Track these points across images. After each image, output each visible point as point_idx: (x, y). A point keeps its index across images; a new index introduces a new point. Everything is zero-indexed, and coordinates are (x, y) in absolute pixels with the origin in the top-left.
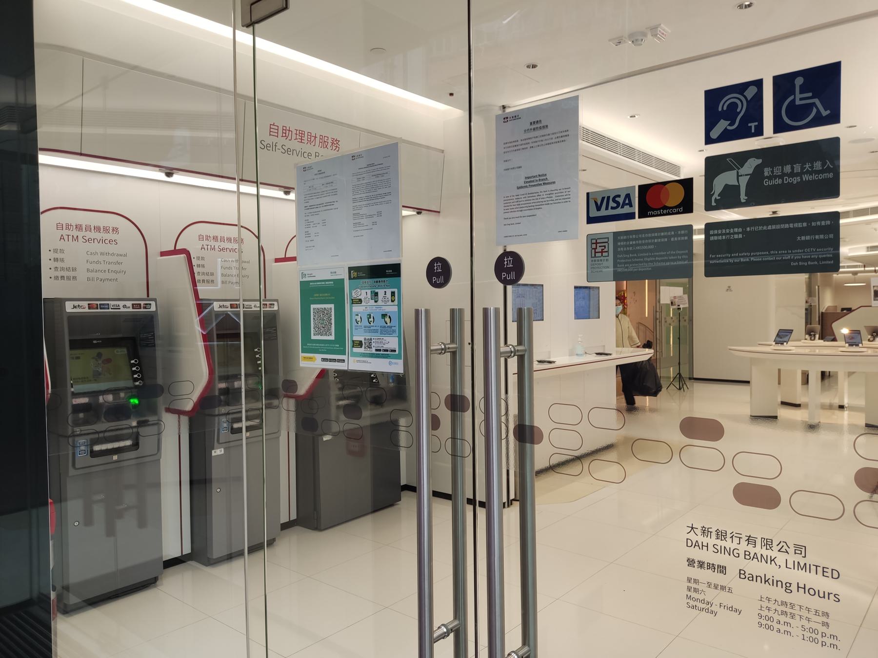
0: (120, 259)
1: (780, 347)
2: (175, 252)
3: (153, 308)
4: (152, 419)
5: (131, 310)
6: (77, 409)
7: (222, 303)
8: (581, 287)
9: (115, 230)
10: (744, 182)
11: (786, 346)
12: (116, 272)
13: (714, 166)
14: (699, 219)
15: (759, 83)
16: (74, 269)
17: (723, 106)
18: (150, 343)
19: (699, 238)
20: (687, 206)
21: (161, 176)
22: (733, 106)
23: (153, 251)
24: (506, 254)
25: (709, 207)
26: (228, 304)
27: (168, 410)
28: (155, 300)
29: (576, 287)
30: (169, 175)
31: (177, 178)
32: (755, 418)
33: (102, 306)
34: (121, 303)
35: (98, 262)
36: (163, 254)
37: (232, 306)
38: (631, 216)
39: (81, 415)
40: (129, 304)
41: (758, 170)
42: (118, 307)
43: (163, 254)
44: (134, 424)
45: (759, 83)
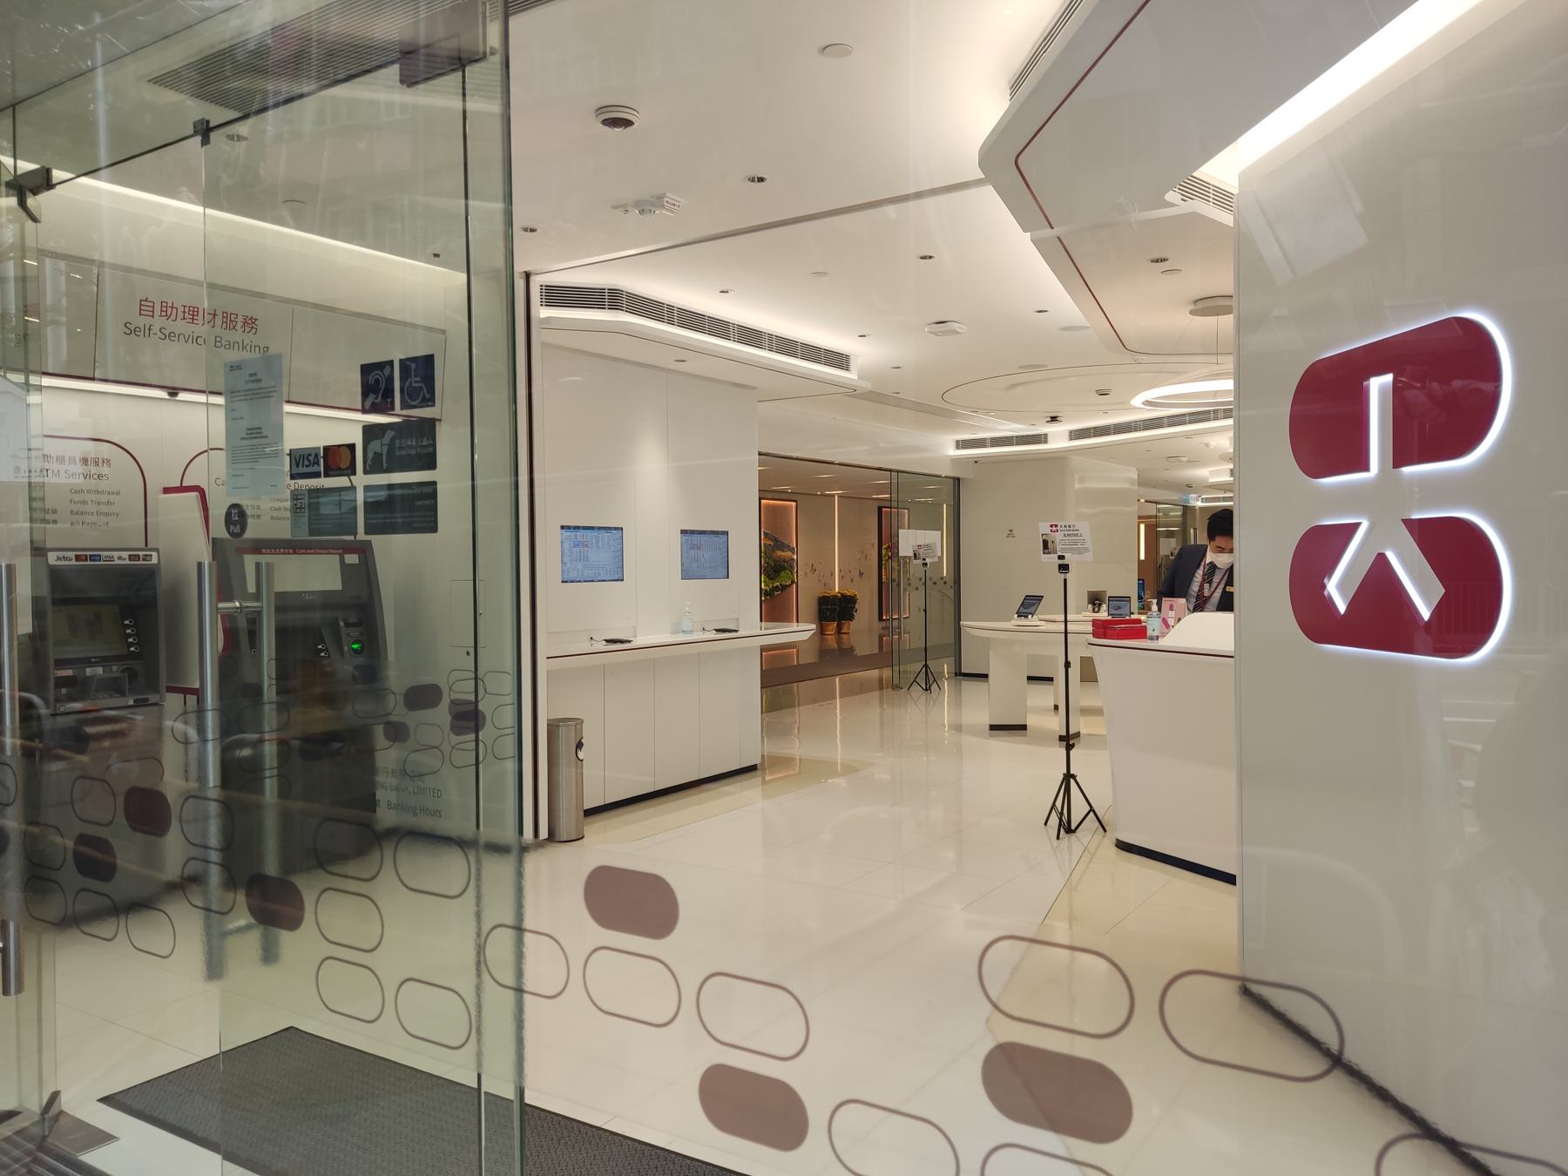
0: (112, 498)
1: (1023, 621)
2: (182, 489)
3: (154, 561)
4: (153, 698)
5: (74, 562)
6: (61, 683)
7: (61, 554)
8: (693, 532)
9: (108, 462)
10: (385, 449)
11: (1032, 621)
12: (107, 514)
13: (370, 432)
14: (361, 480)
15: (391, 363)
16: (55, 511)
17: (371, 379)
18: (151, 604)
19: (360, 497)
20: (352, 470)
21: (163, 394)
22: (377, 381)
23: (154, 486)
24: (234, 506)
25: (366, 472)
26: (72, 554)
27: (170, 689)
28: (157, 550)
29: (683, 532)
30: (173, 392)
31: (182, 396)
32: (993, 728)
33: (92, 558)
34: (116, 554)
35: (84, 502)
36: (167, 490)
37: (78, 558)
38: (317, 475)
39: (64, 691)
40: (125, 554)
41: (393, 440)
42: (111, 559)
43: (167, 490)
44: (131, 702)
45: (391, 363)
